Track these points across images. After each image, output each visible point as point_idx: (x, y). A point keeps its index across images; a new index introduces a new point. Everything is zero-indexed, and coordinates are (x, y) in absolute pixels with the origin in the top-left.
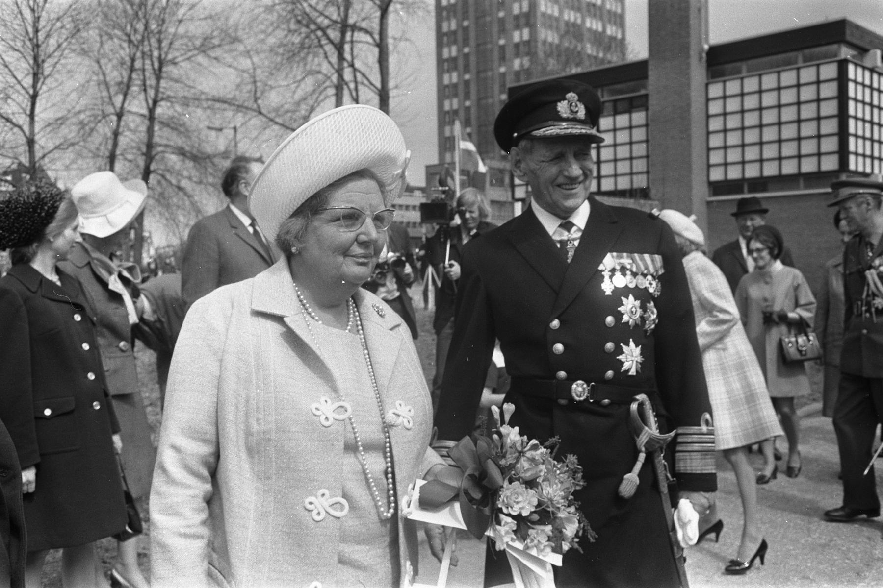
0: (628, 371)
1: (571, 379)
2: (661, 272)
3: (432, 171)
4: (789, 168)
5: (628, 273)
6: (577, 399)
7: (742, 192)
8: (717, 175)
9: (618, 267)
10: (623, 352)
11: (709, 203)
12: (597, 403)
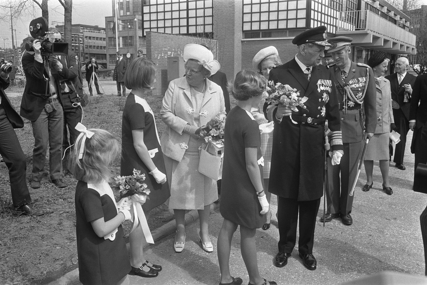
0: (322, 115)
1: (308, 116)
2: (331, 85)
3: (109, 20)
4: (282, 25)
5: (324, 86)
6: (309, 123)
7: (259, 37)
8: (247, 27)
9: (321, 84)
10: (322, 110)
11: (242, 42)
12: (313, 124)
